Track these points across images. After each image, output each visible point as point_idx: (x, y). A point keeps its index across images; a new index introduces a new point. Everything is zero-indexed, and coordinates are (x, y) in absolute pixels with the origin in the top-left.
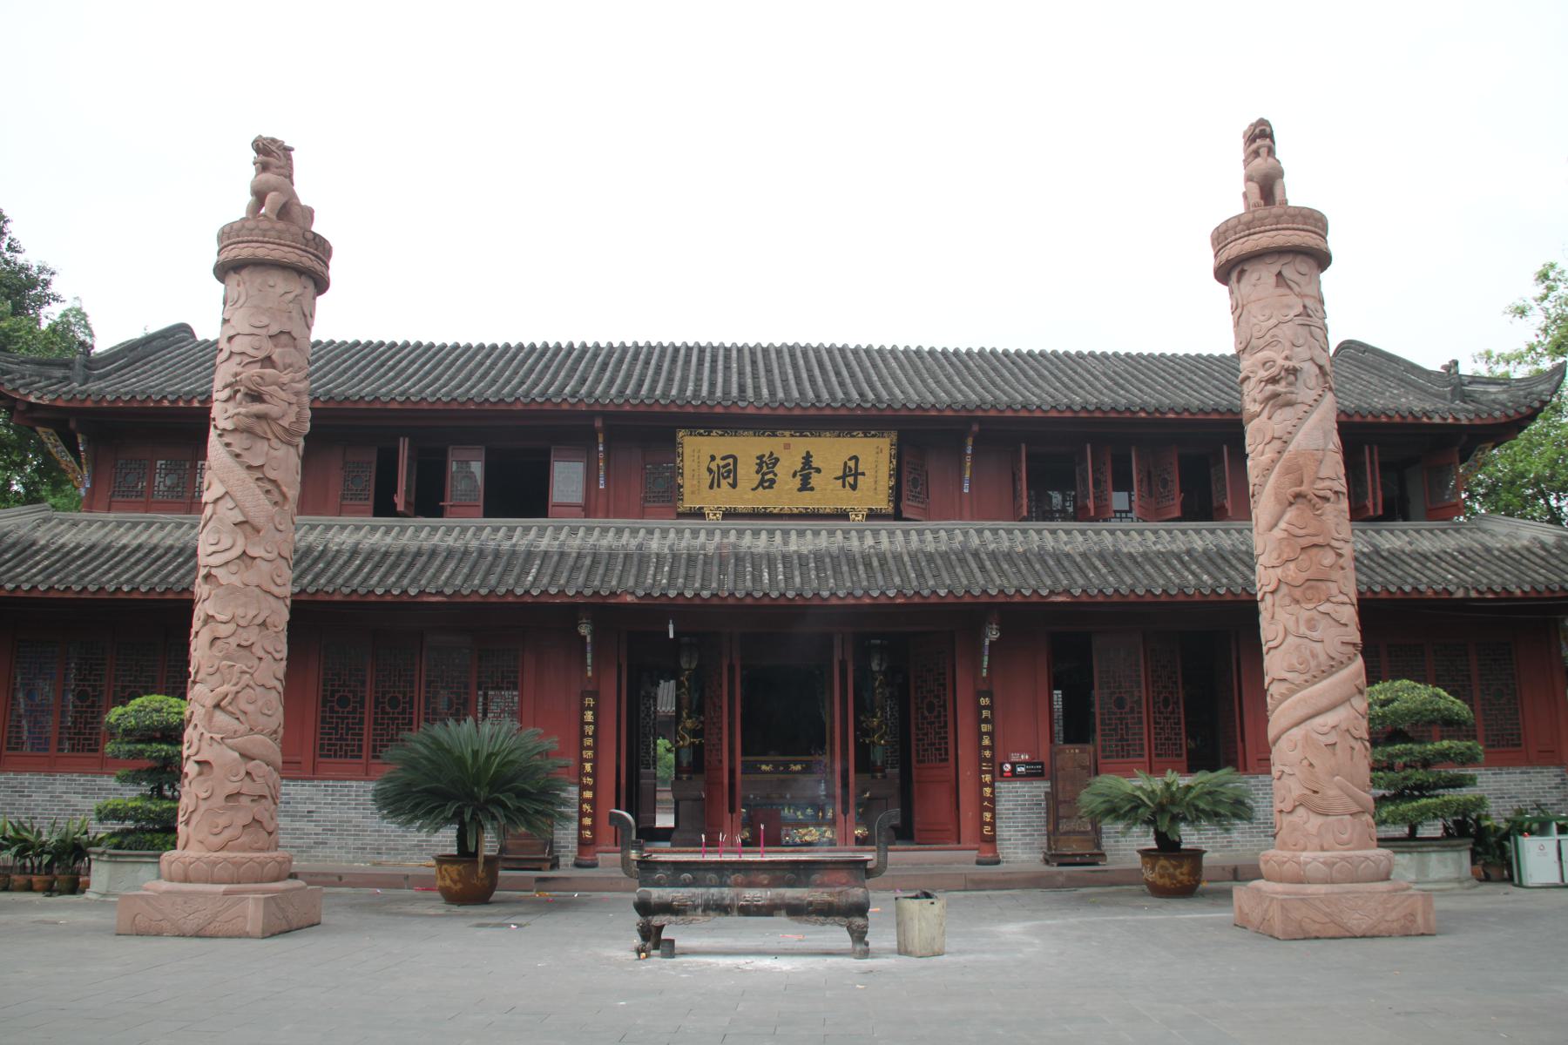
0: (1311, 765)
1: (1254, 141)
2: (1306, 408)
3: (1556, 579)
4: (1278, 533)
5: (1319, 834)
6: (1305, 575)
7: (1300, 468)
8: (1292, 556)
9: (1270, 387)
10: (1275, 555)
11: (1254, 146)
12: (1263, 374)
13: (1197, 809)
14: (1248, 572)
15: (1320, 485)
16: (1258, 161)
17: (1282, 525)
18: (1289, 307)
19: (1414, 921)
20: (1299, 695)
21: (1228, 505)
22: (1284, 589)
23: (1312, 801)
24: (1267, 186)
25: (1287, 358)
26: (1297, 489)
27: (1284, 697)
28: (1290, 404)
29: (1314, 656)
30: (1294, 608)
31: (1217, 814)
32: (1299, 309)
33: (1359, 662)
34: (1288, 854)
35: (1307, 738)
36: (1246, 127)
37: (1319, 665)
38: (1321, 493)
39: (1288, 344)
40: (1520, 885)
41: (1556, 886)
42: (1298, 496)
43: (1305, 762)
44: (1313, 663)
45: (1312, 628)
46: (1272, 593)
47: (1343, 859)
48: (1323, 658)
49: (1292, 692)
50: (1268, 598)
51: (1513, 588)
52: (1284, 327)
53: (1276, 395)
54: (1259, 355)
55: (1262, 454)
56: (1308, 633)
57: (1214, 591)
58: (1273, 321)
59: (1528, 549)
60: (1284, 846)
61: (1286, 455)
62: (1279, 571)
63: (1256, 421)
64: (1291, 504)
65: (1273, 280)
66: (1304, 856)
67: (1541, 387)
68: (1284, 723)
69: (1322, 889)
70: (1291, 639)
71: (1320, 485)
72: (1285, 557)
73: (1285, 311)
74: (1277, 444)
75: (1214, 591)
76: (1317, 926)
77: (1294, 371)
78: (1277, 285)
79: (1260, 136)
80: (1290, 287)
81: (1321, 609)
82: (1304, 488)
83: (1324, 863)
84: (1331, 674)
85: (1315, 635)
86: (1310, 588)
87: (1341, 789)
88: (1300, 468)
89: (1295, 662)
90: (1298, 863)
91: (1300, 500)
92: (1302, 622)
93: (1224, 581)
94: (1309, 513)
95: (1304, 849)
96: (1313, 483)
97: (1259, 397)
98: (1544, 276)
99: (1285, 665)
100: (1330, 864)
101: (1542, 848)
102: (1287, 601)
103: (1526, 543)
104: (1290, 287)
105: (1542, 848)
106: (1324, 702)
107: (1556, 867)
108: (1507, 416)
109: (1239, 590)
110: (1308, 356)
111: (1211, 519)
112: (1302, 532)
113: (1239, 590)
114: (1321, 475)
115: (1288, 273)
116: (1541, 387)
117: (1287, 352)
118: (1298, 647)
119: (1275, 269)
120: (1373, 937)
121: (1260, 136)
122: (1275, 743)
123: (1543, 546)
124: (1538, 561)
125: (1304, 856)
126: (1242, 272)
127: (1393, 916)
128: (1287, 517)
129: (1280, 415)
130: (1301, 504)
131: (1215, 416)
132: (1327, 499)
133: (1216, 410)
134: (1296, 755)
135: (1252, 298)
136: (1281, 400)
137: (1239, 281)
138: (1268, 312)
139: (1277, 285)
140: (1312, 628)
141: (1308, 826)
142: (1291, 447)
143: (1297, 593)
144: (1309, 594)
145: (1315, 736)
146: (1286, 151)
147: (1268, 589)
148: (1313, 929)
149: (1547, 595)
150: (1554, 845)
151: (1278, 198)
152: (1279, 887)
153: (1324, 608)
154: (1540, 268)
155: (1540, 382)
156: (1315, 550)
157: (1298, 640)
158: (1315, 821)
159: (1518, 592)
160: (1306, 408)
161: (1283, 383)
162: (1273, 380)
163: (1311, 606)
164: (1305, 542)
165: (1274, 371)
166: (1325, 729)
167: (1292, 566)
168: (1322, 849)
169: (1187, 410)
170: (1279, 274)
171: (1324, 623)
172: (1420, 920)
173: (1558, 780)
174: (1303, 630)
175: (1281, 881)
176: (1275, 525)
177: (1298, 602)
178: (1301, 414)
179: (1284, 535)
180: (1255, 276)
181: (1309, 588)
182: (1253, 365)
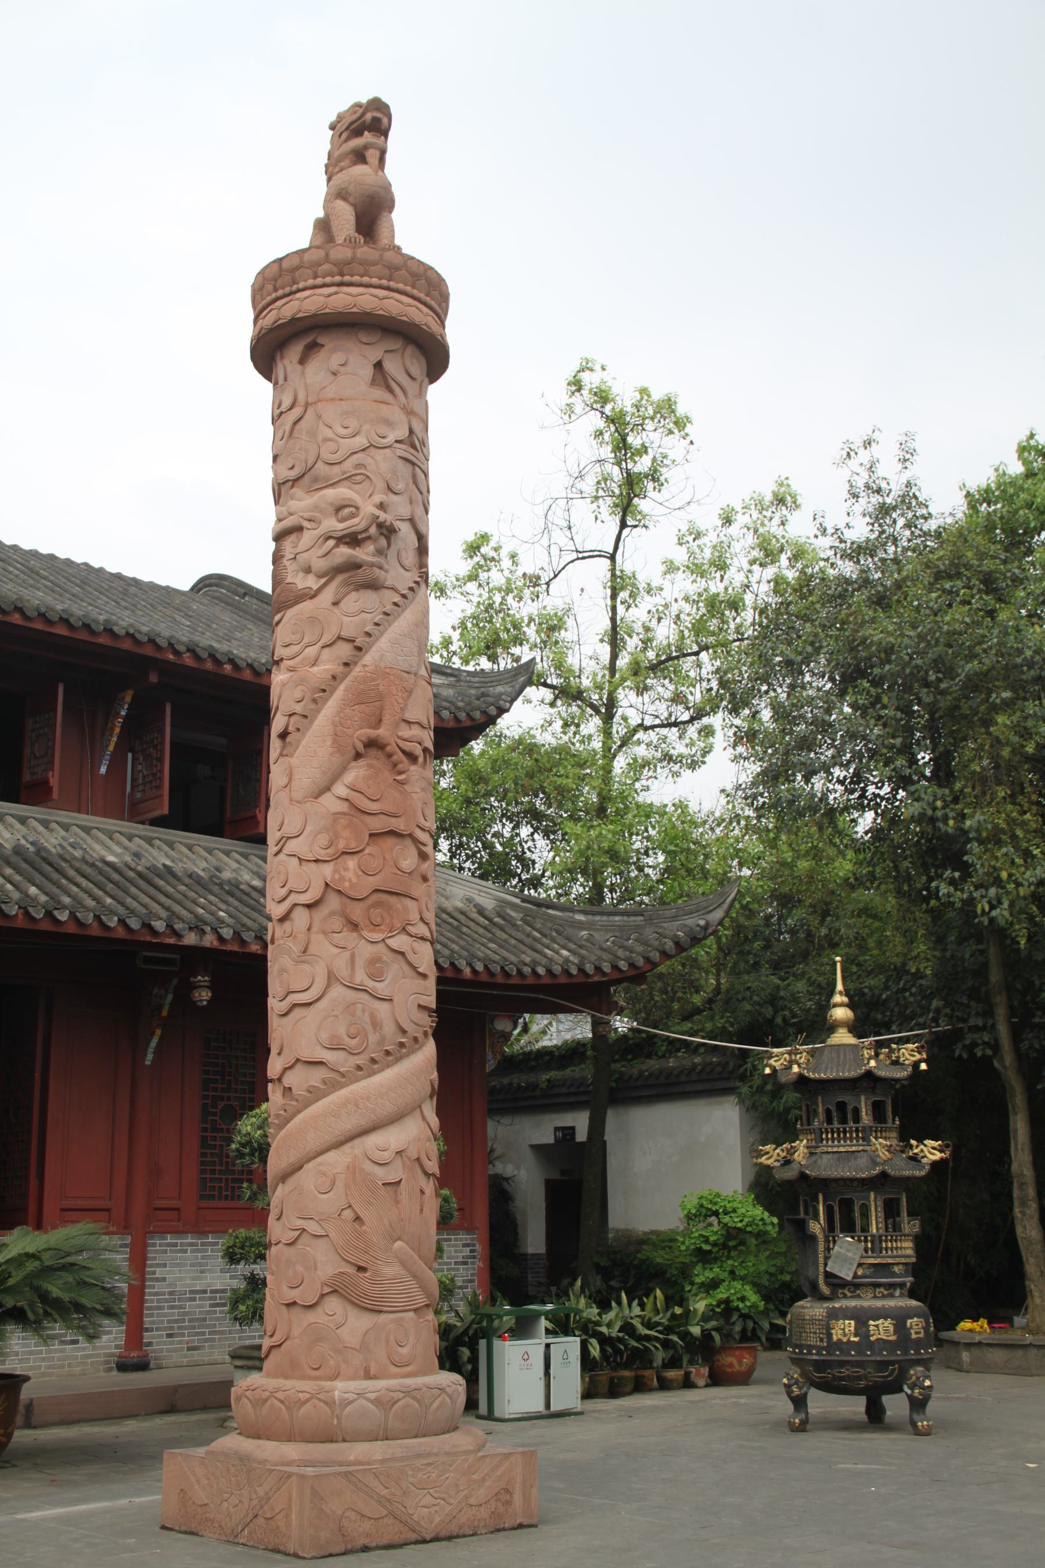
0: (358, 1218)
1: (358, 133)
2: (397, 599)
3: (513, 958)
4: (330, 803)
5: (364, 1347)
6: (373, 882)
7: (380, 698)
8: (354, 846)
9: (345, 551)
10: (323, 839)
11: (357, 142)
12: (333, 524)
13: (44, 1297)
14: (261, 863)
15: (406, 732)
16: (360, 169)
17: (340, 789)
18: (389, 424)
19: (508, 1503)
20: (344, 1092)
21: (54, 781)
22: (333, 902)
23: (353, 1289)
24: (371, 211)
25: (381, 506)
26: (373, 733)
27: (315, 1095)
28: (374, 586)
29: (376, 1024)
30: (348, 937)
31: (79, 1307)
32: (402, 433)
33: (430, 1049)
34: (309, 1386)
35: (353, 1169)
36: (344, 106)
37: (382, 1040)
38: (408, 746)
39: (381, 485)
40: (490, 1416)
41: (538, 1417)
42: (372, 744)
43: (348, 1214)
44: (373, 1038)
45: (376, 976)
46: (309, 906)
47: (408, 1392)
48: (389, 1028)
49: (333, 1086)
50: (301, 917)
51: (462, 964)
52: (379, 455)
53: (352, 566)
54: (330, 493)
55: (315, 663)
56: (370, 984)
57: (49, 914)
58: (360, 441)
59: (462, 913)
60: (292, 1370)
61: (357, 671)
62: (327, 870)
63: (306, 606)
64: (358, 756)
65: (368, 372)
66: (342, 1389)
67: (500, 689)
68: (312, 1141)
69: (377, 1450)
70: (337, 992)
71: (406, 732)
72: (341, 845)
73: (383, 430)
74: (344, 650)
75: (49, 914)
76: (367, 1525)
77: (388, 531)
78: (373, 383)
79: (364, 130)
80: (391, 391)
81: (393, 943)
82: (382, 732)
83: (377, 1402)
84: (399, 1059)
85: (381, 988)
86: (365, 909)
87: (403, 1264)
88: (380, 698)
89: (342, 1031)
90: (330, 1403)
91: (373, 752)
92: (360, 963)
93: (66, 900)
94: (388, 776)
95: (335, 1377)
96: (397, 726)
97: (320, 565)
98: (473, 549)
99: (324, 1036)
100: (383, 1403)
101: (526, 1357)
102: (337, 923)
103: (460, 905)
104: (391, 391)
105: (526, 1357)
106: (388, 1108)
107: (541, 1384)
108: (457, 719)
109: (90, 919)
110: (407, 514)
111: (16, 800)
112: (373, 807)
113: (90, 919)
114: (409, 716)
115: (392, 366)
116: (500, 689)
117: (378, 498)
118: (350, 1006)
119: (375, 354)
120: (450, 1538)
121: (364, 130)
122: (284, 1177)
123: (481, 911)
124: (481, 931)
125: (342, 1389)
126: (313, 347)
127: (481, 1494)
128: (349, 777)
129: (355, 601)
130: (374, 759)
131: (62, 631)
132: (412, 758)
133: (65, 621)
134: (331, 1202)
135: (329, 393)
136: (361, 575)
137: (302, 361)
138: (353, 423)
139: (373, 383)
140: (376, 976)
141: (343, 1332)
142: (368, 659)
143: (357, 912)
144: (376, 914)
145: (369, 1167)
146: (404, 163)
147: (304, 899)
148: (360, 1531)
149: (500, 979)
150: (542, 1348)
151: (384, 241)
152: (291, 1451)
153: (399, 942)
154: (471, 538)
155: (500, 682)
156: (390, 841)
157: (352, 995)
158: (355, 1325)
159: (467, 971)
160: (397, 599)
161: (370, 548)
162: (353, 540)
163: (377, 936)
164: (378, 824)
165: (357, 523)
166: (386, 1156)
167: (351, 863)
168: (368, 1376)
169: (20, 610)
170: (378, 365)
171: (395, 968)
172: (518, 1499)
173: (467, 1251)
174: (361, 977)
175: (289, 1438)
176: (328, 789)
177: (355, 926)
178: (389, 608)
179: (344, 807)
180: (336, 359)
181: (378, 904)
182: (316, 508)
